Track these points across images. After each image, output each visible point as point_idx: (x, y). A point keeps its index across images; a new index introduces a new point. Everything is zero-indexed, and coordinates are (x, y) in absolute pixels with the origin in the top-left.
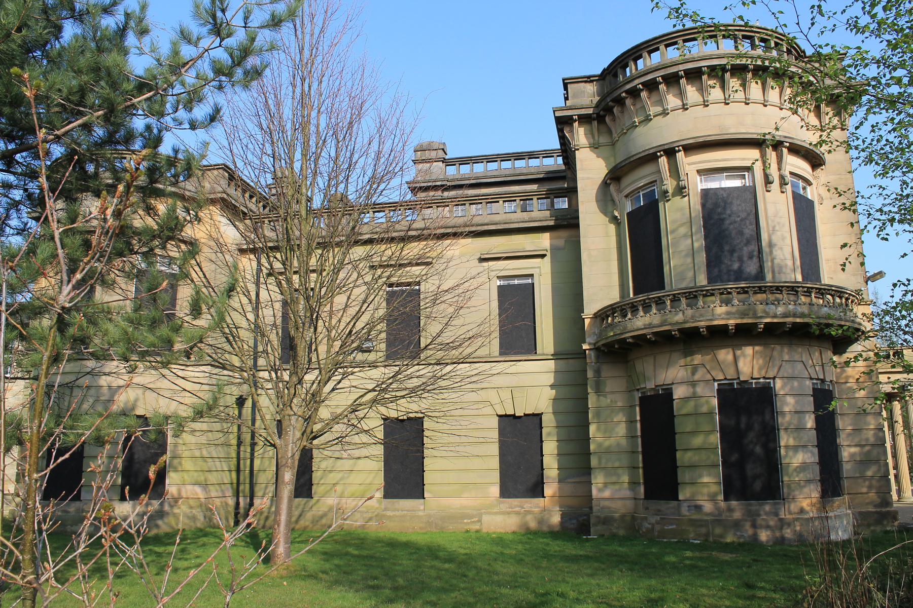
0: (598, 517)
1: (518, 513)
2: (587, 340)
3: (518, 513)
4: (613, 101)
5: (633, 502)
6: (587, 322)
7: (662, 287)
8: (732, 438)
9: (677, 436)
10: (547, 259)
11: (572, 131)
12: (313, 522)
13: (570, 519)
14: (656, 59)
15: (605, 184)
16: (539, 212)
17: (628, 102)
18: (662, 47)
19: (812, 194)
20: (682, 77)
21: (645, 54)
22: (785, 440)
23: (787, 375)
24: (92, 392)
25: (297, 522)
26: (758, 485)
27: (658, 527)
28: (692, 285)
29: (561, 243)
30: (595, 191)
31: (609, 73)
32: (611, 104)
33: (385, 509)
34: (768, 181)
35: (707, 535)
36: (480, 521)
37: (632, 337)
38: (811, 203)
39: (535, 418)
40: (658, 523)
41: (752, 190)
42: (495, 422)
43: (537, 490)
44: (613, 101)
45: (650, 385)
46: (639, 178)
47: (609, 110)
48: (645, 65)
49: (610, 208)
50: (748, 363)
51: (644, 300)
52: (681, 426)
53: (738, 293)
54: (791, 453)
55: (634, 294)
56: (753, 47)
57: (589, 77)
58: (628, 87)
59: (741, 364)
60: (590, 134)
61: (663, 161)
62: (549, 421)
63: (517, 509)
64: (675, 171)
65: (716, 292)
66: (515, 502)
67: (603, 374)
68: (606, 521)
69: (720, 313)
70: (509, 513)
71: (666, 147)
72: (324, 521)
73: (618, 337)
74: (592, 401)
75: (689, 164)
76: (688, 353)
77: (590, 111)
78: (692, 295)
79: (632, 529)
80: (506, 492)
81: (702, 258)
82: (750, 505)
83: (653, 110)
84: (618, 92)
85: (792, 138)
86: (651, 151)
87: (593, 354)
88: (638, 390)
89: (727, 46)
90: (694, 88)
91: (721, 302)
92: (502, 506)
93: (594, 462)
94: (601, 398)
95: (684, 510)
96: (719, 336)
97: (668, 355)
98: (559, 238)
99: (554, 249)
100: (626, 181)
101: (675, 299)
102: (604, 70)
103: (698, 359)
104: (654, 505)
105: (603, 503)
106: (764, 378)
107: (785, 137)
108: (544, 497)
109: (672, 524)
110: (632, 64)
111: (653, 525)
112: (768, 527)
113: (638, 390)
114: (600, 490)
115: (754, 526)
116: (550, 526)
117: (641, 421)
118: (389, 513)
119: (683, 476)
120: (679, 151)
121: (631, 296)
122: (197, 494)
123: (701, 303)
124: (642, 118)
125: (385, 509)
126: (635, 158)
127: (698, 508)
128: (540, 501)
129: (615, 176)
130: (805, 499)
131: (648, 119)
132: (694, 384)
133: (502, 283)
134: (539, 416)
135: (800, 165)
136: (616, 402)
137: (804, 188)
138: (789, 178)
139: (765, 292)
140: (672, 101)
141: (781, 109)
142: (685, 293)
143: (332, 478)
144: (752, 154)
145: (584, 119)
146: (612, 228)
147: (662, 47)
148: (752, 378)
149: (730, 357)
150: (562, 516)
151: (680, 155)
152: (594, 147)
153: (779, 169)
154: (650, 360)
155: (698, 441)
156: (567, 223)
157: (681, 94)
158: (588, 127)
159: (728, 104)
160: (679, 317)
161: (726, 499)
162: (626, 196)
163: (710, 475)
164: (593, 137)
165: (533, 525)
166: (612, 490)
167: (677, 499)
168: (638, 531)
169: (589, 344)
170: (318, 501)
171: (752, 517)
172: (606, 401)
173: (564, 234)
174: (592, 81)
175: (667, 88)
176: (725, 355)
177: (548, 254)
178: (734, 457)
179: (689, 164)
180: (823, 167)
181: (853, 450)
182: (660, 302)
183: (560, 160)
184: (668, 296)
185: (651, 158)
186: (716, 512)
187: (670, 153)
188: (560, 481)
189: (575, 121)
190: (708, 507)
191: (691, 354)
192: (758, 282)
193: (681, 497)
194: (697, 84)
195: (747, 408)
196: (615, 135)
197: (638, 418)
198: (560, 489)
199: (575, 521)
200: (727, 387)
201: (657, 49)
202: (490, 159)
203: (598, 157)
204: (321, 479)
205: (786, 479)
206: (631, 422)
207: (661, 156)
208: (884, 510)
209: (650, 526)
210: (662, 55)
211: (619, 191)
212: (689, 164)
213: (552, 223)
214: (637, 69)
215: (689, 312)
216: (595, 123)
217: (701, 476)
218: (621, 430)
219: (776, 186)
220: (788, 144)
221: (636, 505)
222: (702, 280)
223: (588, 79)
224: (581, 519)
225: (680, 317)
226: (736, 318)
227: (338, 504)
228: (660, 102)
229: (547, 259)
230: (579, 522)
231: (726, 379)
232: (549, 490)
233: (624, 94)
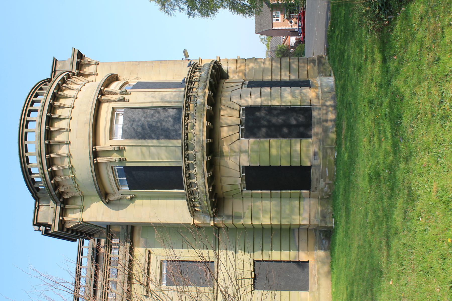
0: (321, 221)
1: (319, 279)
2: (208, 222)
3: (319, 279)
4: (55, 190)
5: (311, 199)
6: (197, 222)
7: (179, 169)
8: (274, 132)
9: (272, 165)
10: (152, 250)
11: (70, 222)
13: (323, 244)
14: (33, 160)
15: (108, 203)
16: (119, 252)
17: (58, 179)
18: (26, 154)
19: (134, 82)
20: (49, 142)
21: (29, 166)
22: (276, 103)
23: (237, 101)
26: (301, 119)
27: (328, 181)
28: (180, 148)
29: (142, 241)
30: (112, 211)
31: (36, 194)
32: (57, 192)
34: (123, 100)
35: (331, 149)
37: (209, 187)
38: (138, 83)
39: (256, 265)
40: (324, 181)
41: (127, 109)
43: (303, 265)
44: (55, 190)
45: (239, 181)
46: (108, 177)
47: (61, 195)
48: (36, 167)
49: (124, 202)
50: (230, 117)
51: (186, 177)
52: (265, 162)
53: (188, 119)
54: (284, 100)
55: (183, 189)
56: (39, 102)
57: (36, 208)
58: (48, 178)
59: (229, 122)
60: (74, 210)
61: (100, 160)
62: (258, 256)
63: (316, 279)
64: (108, 153)
65: (186, 132)
66: (311, 281)
67: (230, 213)
68: (324, 217)
69: (198, 128)
70: (319, 285)
71: (92, 156)
73: (208, 197)
74: (249, 222)
75: (104, 143)
76: (221, 154)
77: (59, 208)
78: (186, 147)
79: (329, 198)
80: (305, 288)
81: (164, 142)
82: (314, 123)
83: (66, 163)
84: (50, 185)
85: (99, 85)
86: (93, 166)
87: (217, 219)
88: (242, 191)
90: (58, 136)
91: (193, 129)
92: (314, 290)
93: (285, 222)
94: (245, 216)
95: (316, 163)
96: (212, 132)
97: (222, 167)
98: (139, 241)
99: (146, 245)
100: (109, 189)
101: (187, 157)
102: (33, 196)
103: (226, 149)
104: (314, 183)
105: (312, 218)
106: (240, 111)
107: (98, 88)
108: (308, 262)
109: (326, 171)
110: (32, 176)
111: (326, 184)
112: (326, 114)
113: (242, 191)
114: (304, 219)
115: (326, 121)
116: (327, 257)
117: (261, 190)
119: (296, 162)
120: (95, 148)
121: (184, 191)
123: (192, 142)
124: (70, 172)
126: (95, 178)
129: (104, 195)
130: (310, 95)
131: (71, 168)
132: (240, 152)
133: (164, 282)
134: (255, 262)
135: (115, 86)
136: (249, 206)
137: (130, 85)
138: (123, 89)
139: (189, 105)
140: (63, 150)
141: (80, 90)
142: (185, 151)
144: (106, 109)
145: (63, 212)
146: (137, 201)
147: (26, 154)
148: (239, 117)
149: (226, 129)
151: (98, 148)
152: (83, 209)
153: (116, 94)
154: (224, 179)
155: (274, 152)
156: (130, 232)
157: (60, 144)
158: (69, 212)
159: (71, 118)
160: (199, 155)
161: (310, 137)
162: (119, 190)
163: (296, 145)
164: (76, 209)
165: (326, 268)
166: (303, 211)
167: (309, 168)
168: (330, 195)
169: (211, 221)
171: (320, 122)
172: (247, 213)
173: (136, 238)
174: (39, 206)
175: (53, 153)
176: (224, 132)
177: (150, 249)
178: (285, 130)
179: (105, 144)
180: (119, 75)
181: (283, 73)
182: (188, 167)
183: (86, 242)
184: (185, 161)
185: (97, 166)
186: (318, 143)
187: (96, 154)
189: (63, 219)
190: (315, 148)
191: (222, 152)
192: (181, 113)
193: (309, 164)
194: (55, 134)
195: (256, 122)
196: (77, 194)
197: (260, 191)
199: (324, 241)
200: (244, 133)
201: (27, 157)
202: (80, 261)
203: (89, 207)
205: (299, 104)
206: (262, 197)
207: (97, 160)
208: (317, 62)
209: (327, 186)
210: (32, 154)
211: (114, 194)
212: (105, 144)
213: (128, 244)
214: (37, 174)
215: (197, 148)
216: (67, 206)
217: (296, 151)
218: (267, 204)
219: (127, 97)
220: (103, 88)
221: (314, 197)
222: (179, 142)
223: (37, 208)
224: (322, 238)
225: (199, 154)
226: (203, 118)
228: (62, 158)
229: (152, 250)
230: (325, 236)
231: (239, 133)
232: (303, 257)
233: (52, 181)
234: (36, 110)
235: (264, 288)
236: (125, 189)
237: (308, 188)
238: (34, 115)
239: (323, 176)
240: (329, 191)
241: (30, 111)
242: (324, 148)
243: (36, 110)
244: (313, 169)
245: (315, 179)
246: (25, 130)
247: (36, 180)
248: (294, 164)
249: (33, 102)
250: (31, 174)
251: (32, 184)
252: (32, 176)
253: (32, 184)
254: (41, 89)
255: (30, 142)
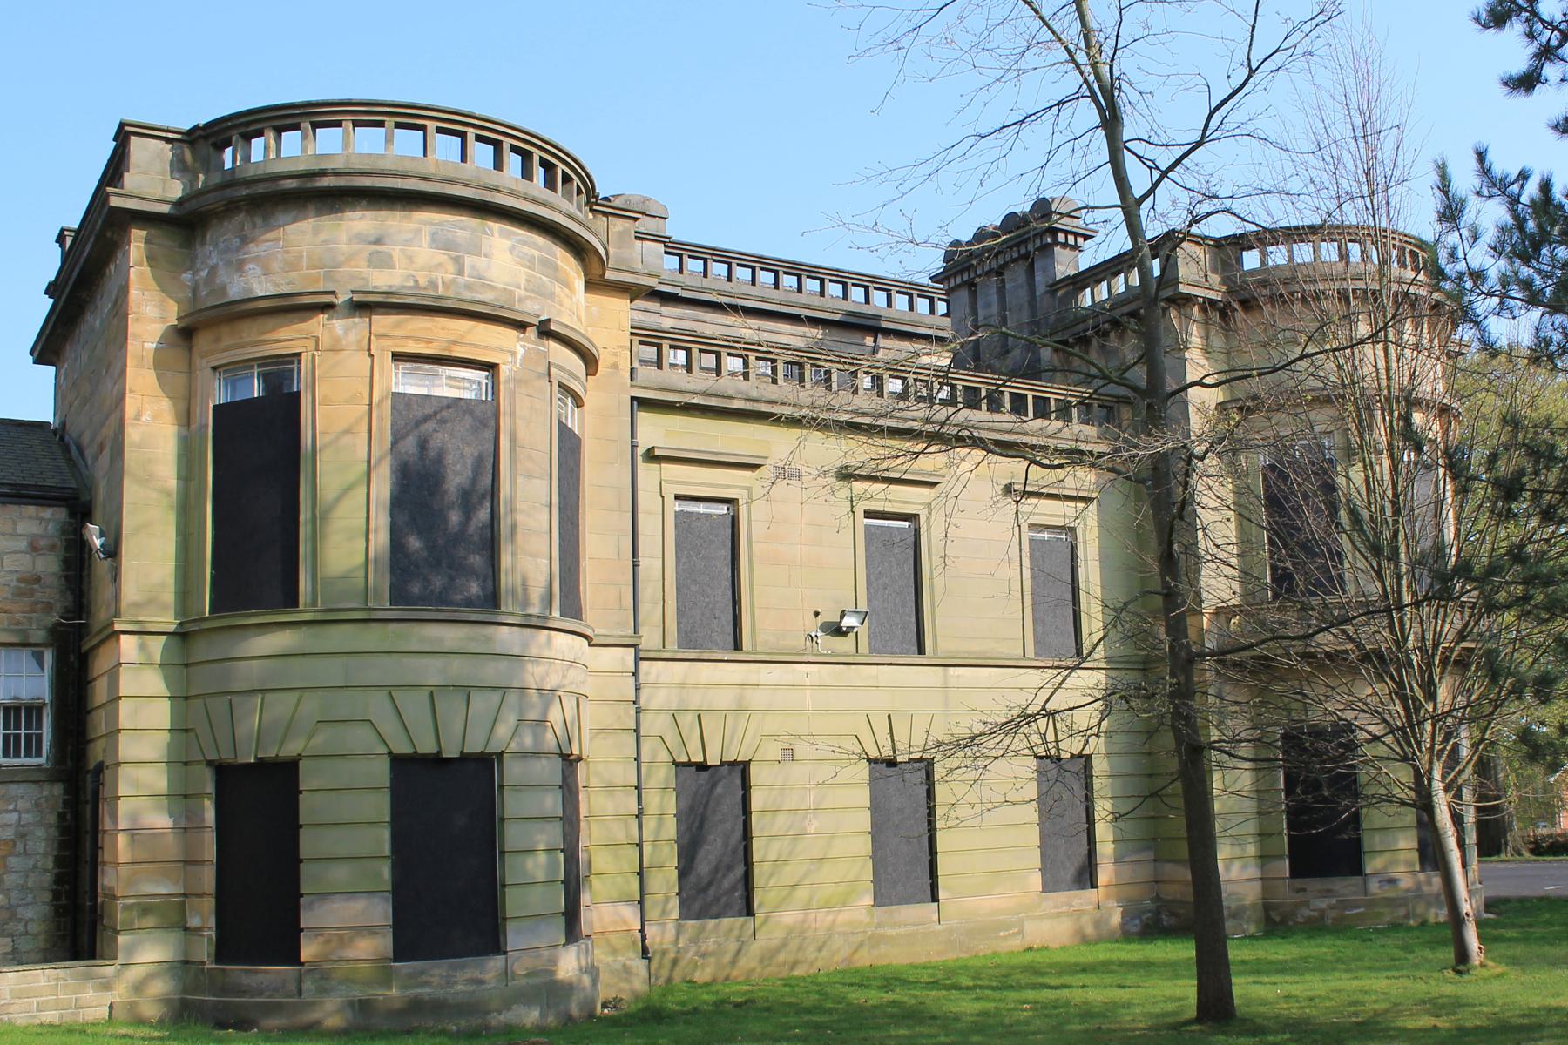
12: (761, 961)
14: (328, 142)
24: (512, 698)
25: (734, 962)
31: (206, 138)
33: (879, 925)
36: (1021, 932)
40: (1332, 907)
42: (381, 771)
43: (1086, 876)
56: (527, 174)
62: (1100, 766)
66: (1062, 896)
70: (1058, 915)
72: (782, 957)
89: (446, 147)
95: (1374, 886)
102: (196, 128)
111: (1322, 911)
118: (890, 932)
119: (1370, 841)
122: (625, 922)
125: (879, 925)
127: (1392, 881)
128: (1091, 894)
143: (789, 873)
150: (1124, 914)
161: (1423, 870)
162: (214, 368)
170: (767, 919)
188: (1116, 862)
190: (1406, 882)
193: (1368, 871)
198: (1117, 874)
204: (772, 875)
227: (804, 921)
229: (1093, 506)
232: (1104, 875)
234: (498, 164)
235: (873, 782)
236: (218, 394)
237: (1296, 872)
238: (482, 154)
239: (1344, 904)
240: (1300, 920)
241: (497, 145)
242: (1405, 899)
243: (498, 164)
244: (1359, 878)
245: (1330, 886)
246: (390, 121)
247: (257, 144)
248: (304, 836)
249: (526, 156)
250: (279, 131)
251: (243, 130)
252: (271, 135)
253: (243, 130)
254: (567, 179)
255: (389, 140)
